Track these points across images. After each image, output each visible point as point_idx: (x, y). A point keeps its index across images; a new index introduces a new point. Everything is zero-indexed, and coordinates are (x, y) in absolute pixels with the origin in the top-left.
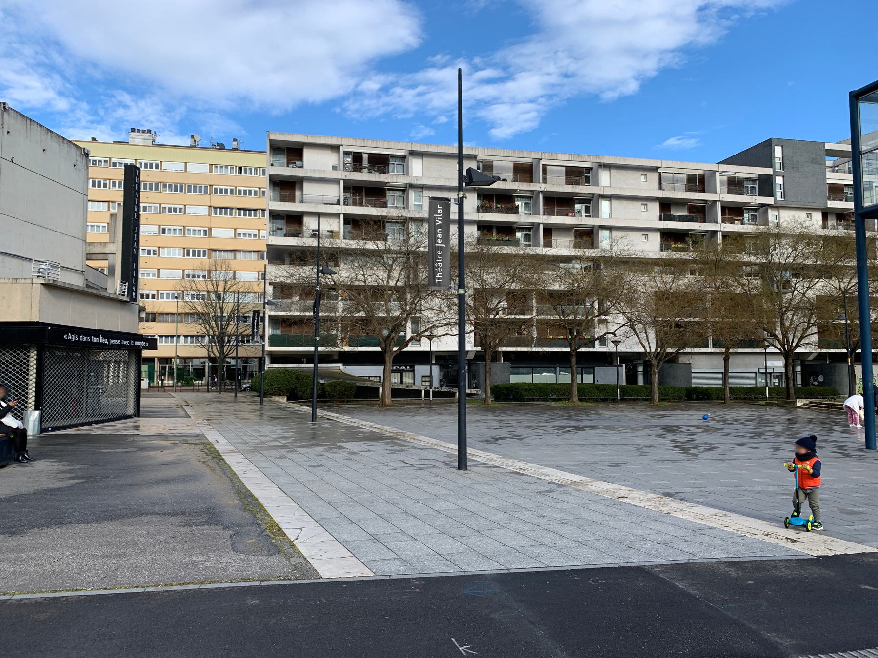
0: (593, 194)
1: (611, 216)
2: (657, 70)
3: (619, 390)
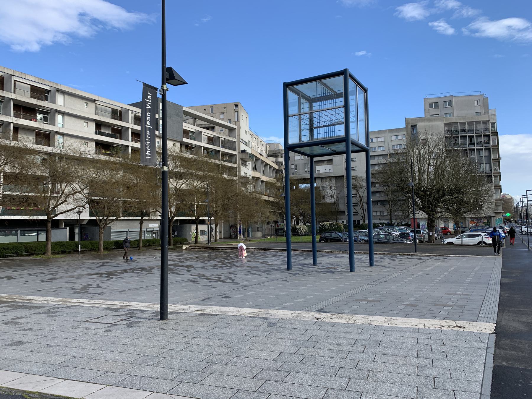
0: (51, 109)
1: (63, 126)
2: (53, 42)
3: (80, 245)
